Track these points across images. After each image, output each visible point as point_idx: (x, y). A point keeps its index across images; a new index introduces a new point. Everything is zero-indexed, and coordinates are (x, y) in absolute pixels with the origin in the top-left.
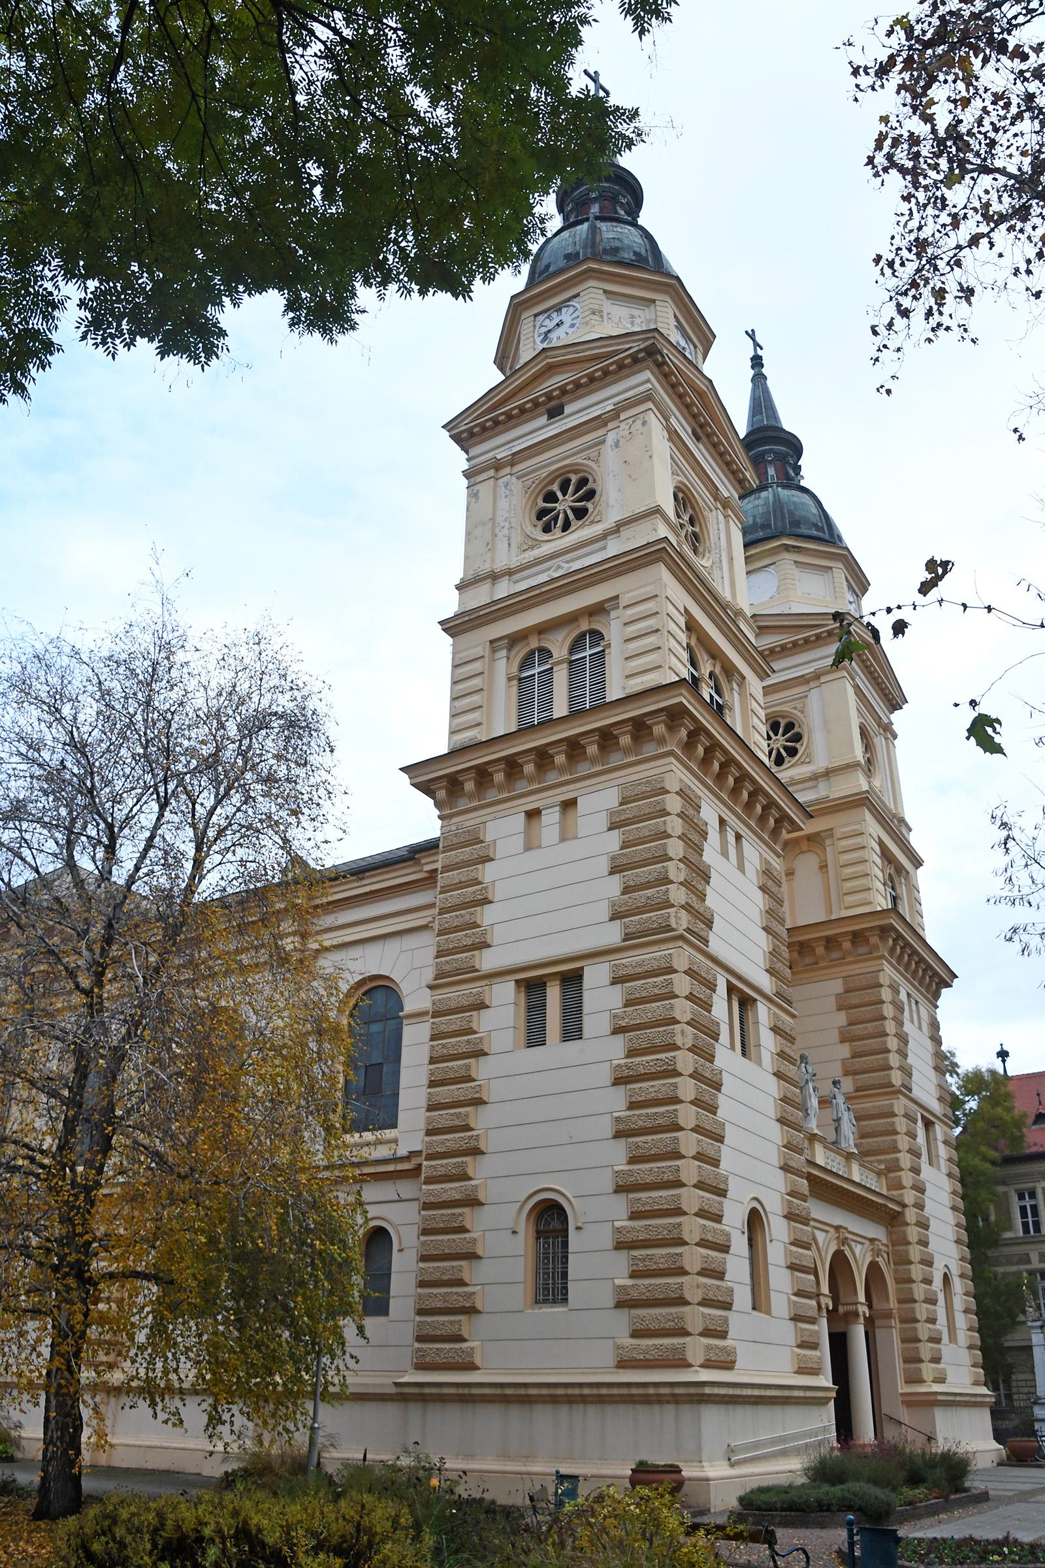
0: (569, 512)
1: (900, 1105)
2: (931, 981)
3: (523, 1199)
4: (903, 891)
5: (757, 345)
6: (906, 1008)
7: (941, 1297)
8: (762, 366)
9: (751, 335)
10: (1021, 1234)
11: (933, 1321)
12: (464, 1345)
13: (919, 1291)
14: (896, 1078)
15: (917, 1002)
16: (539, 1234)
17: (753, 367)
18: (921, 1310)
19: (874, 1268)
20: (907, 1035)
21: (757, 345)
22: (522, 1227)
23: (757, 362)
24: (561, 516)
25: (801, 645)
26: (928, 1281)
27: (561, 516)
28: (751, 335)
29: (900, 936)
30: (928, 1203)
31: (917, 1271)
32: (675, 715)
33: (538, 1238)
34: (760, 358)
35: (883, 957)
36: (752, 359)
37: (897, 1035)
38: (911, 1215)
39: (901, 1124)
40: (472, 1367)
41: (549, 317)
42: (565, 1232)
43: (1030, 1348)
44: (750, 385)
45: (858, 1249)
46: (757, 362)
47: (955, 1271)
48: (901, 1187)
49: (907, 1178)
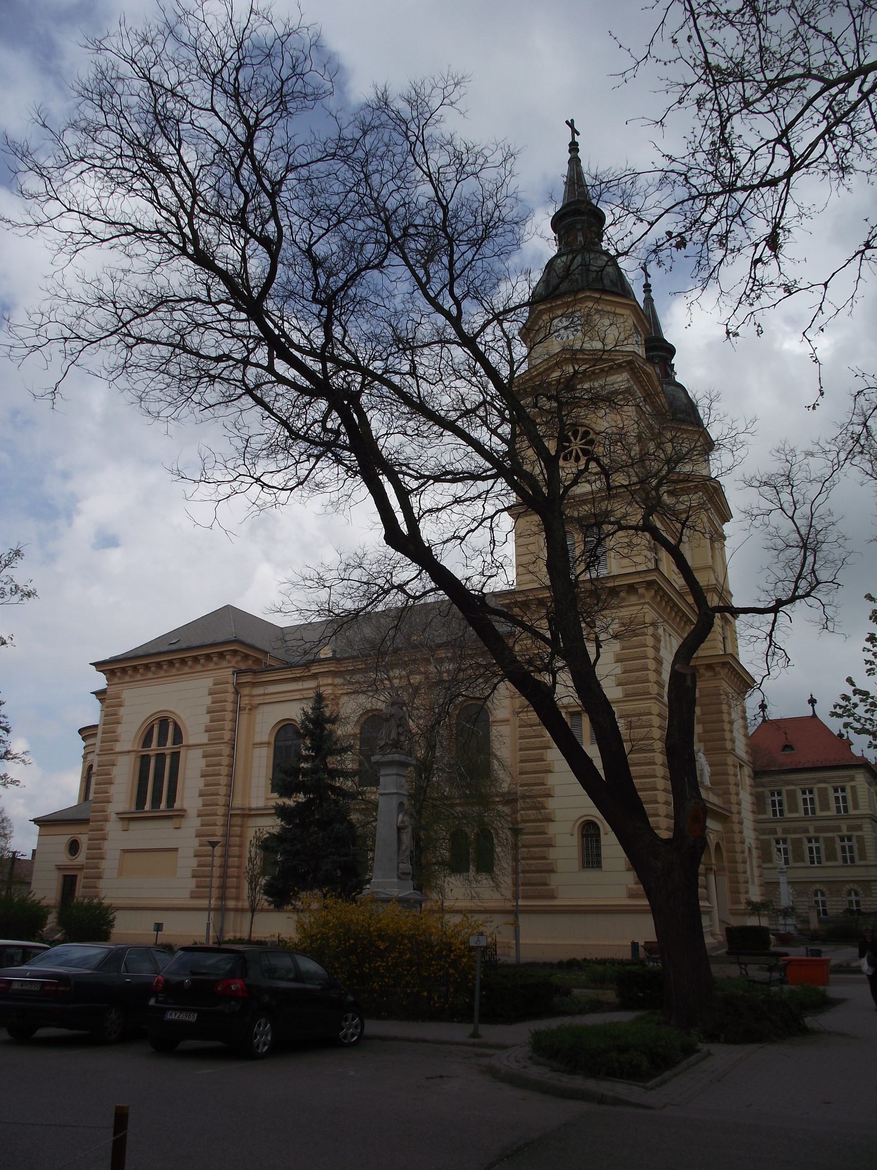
0: (579, 451)
1: (730, 760)
2: (661, 600)
3: (575, 818)
4: (728, 634)
5: (575, 132)
6: (662, 639)
7: (748, 860)
8: (578, 151)
9: (571, 124)
10: (771, 816)
11: (745, 872)
12: (547, 887)
13: (739, 857)
14: (729, 745)
15: (670, 635)
16: (583, 836)
17: (570, 151)
18: (740, 868)
19: (718, 846)
20: (662, 658)
21: (575, 132)
22: (576, 832)
23: (574, 147)
24: (574, 452)
25: (598, 373)
26: (743, 852)
27: (574, 452)
28: (571, 124)
29: (660, 588)
30: (743, 811)
31: (738, 848)
32: (650, 584)
33: (582, 838)
34: (577, 144)
35: (722, 679)
36: (570, 145)
37: (655, 659)
38: (735, 818)
39: (731, 770)
40: (553, 897)
41: (560, 321)
42: (599, 835)
43: (778, 883)
44: (567, 166)
45: (711, 836)
46: (574, 147)
47: (753, 845)
48: (730, 803)
49: (733, 799)
